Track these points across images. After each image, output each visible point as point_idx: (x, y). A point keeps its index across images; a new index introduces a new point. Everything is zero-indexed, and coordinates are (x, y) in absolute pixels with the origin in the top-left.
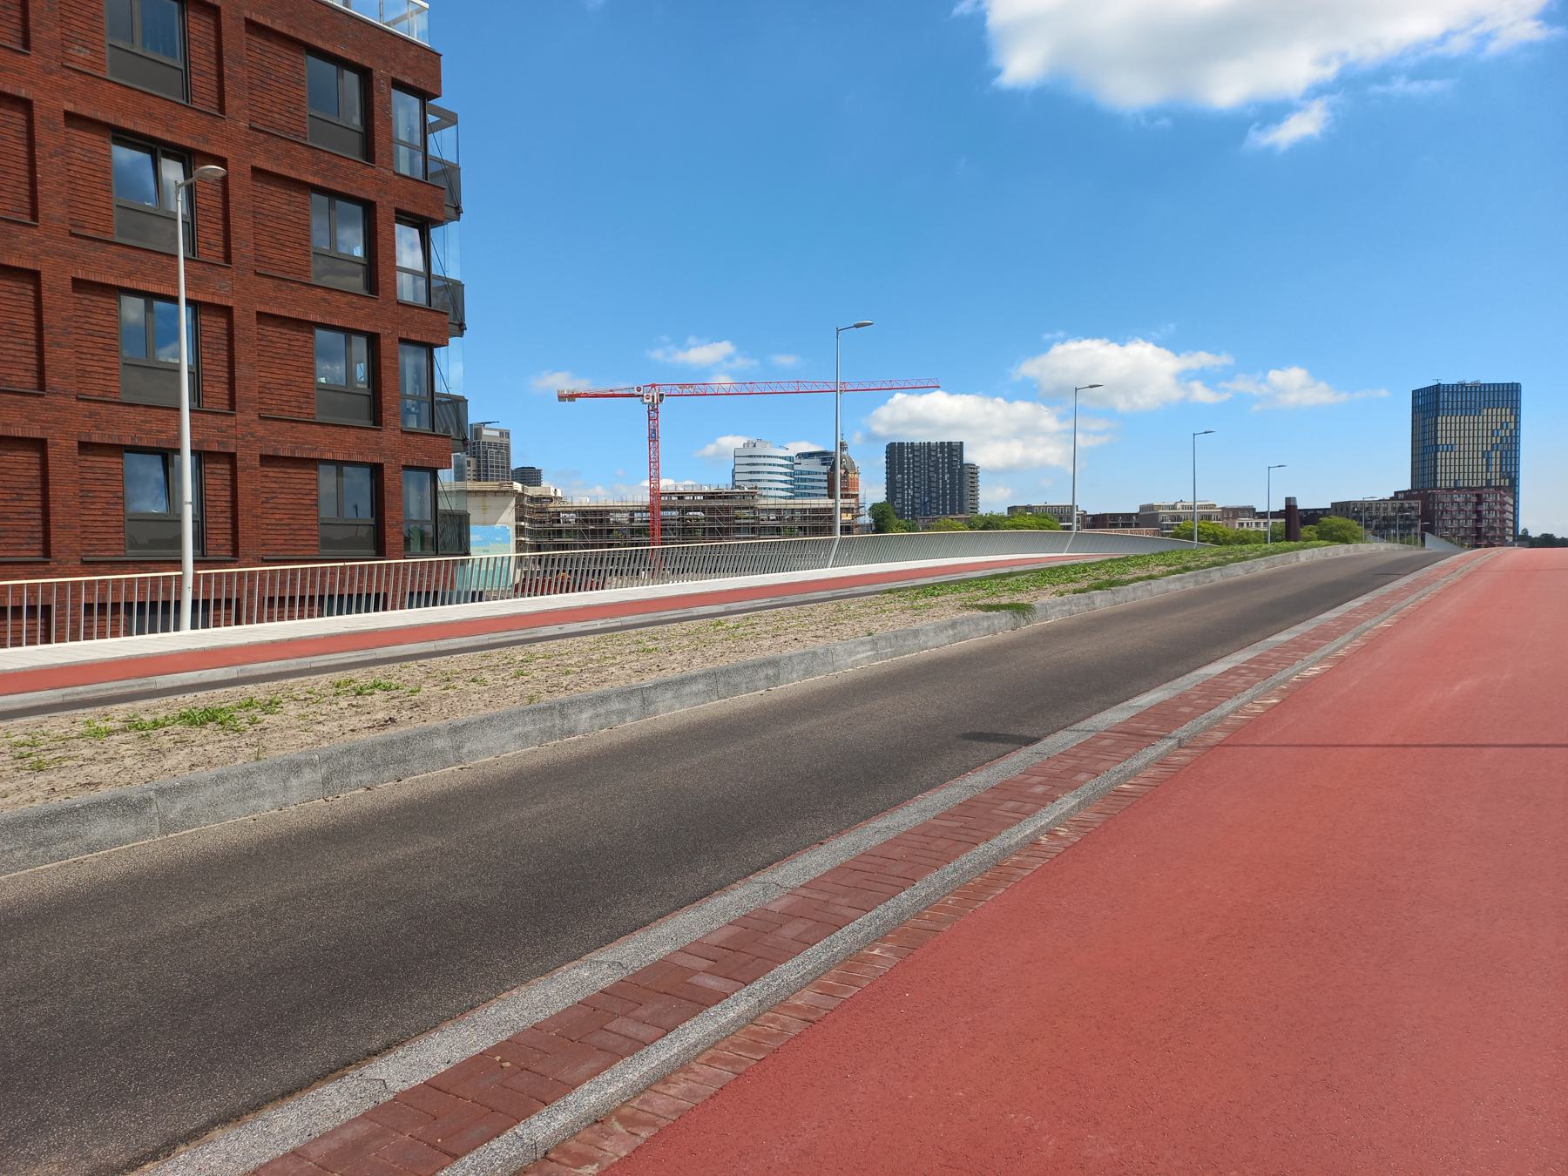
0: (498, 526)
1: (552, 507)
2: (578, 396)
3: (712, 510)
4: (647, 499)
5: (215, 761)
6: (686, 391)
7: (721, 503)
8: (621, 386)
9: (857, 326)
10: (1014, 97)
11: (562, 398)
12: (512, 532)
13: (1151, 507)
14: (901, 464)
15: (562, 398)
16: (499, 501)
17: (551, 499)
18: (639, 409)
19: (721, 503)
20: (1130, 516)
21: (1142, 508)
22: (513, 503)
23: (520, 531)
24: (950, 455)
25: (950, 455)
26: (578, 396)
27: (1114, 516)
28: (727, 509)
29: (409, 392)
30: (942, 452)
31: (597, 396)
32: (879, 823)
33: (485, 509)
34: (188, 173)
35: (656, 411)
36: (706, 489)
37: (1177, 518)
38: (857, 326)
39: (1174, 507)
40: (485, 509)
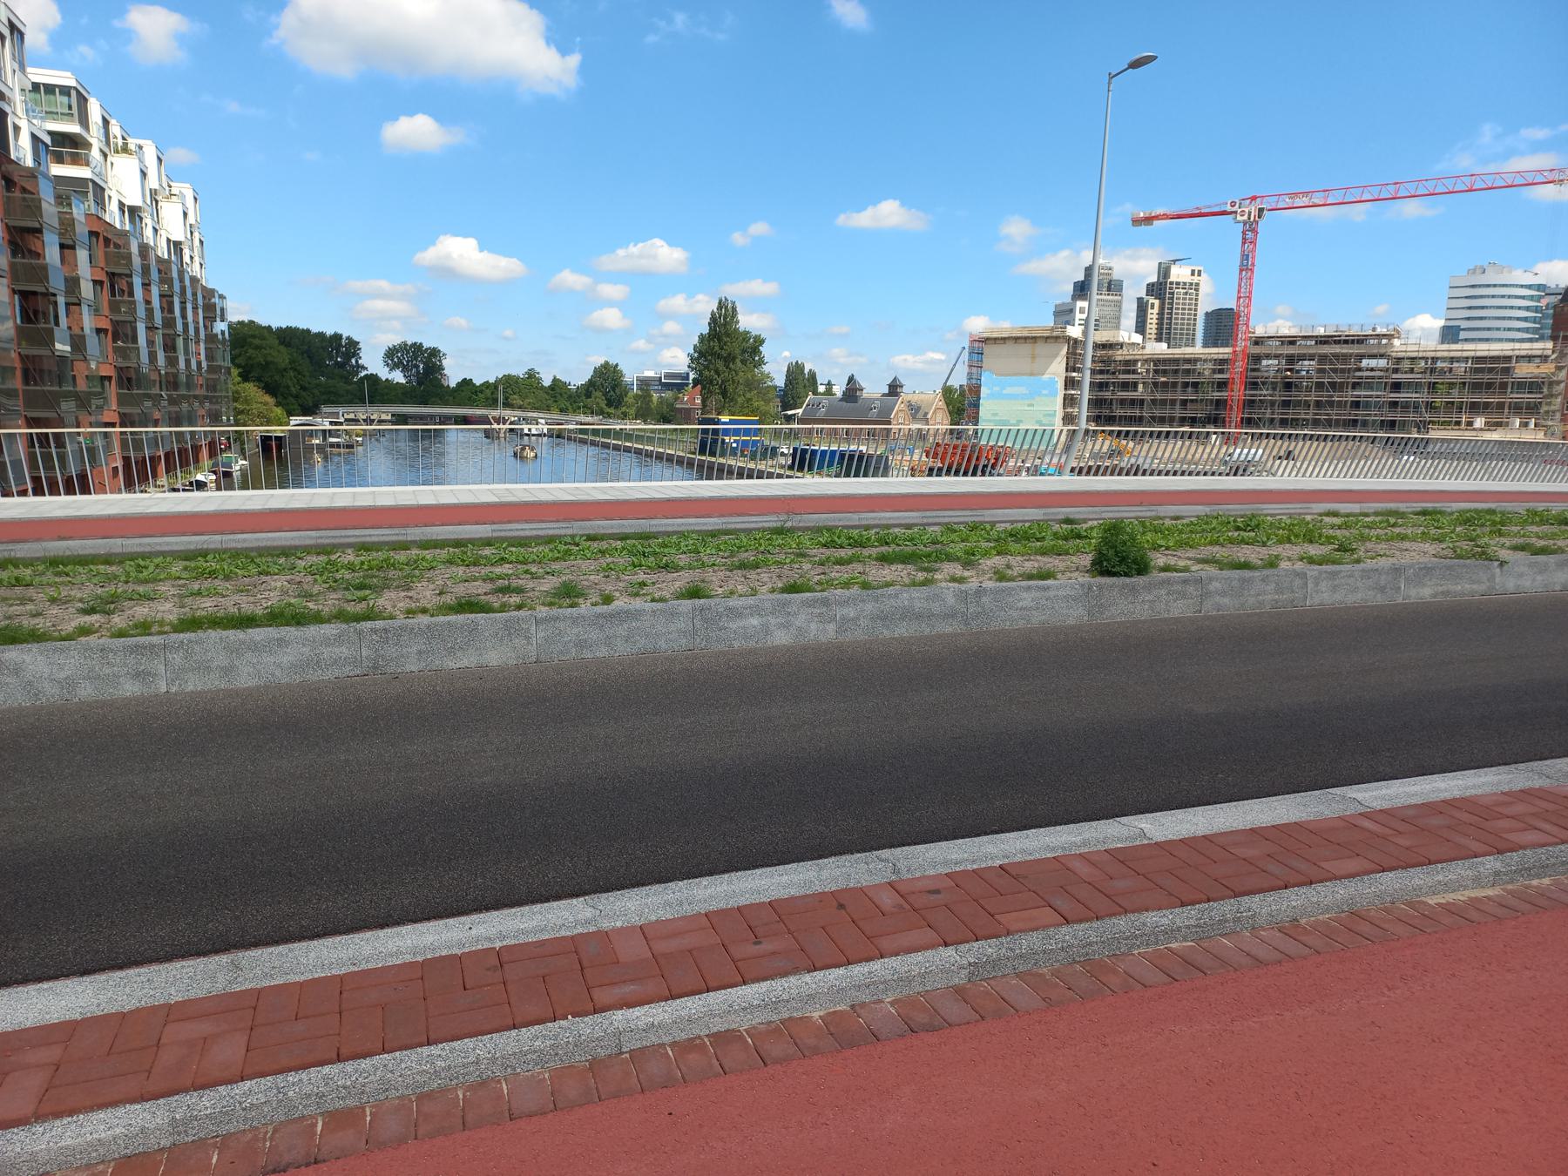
0: (1046, 377)
1: (1120, 355)
2: (1157, 217)
3: (1323, 358)
4: (677, 359)
5: (569, 622)
6: (1298, 202)
7: (1337, 349)
8: (1205, 204)
9: (1136, 64)
11: (1137, 222)
15: (1137, 222)
16: (1051, 347)
17: (1121, 345)
18: (1229, 231)
19: (1337, 349)
26: (1157, 217)
28: (1345, 358)
31: (1179, 217)
32: (437, 1051)
33: (1033, 357)
35: (1255, 231)
36: (1321, 331)
38: (1136, 64)
40: (1033, 357)
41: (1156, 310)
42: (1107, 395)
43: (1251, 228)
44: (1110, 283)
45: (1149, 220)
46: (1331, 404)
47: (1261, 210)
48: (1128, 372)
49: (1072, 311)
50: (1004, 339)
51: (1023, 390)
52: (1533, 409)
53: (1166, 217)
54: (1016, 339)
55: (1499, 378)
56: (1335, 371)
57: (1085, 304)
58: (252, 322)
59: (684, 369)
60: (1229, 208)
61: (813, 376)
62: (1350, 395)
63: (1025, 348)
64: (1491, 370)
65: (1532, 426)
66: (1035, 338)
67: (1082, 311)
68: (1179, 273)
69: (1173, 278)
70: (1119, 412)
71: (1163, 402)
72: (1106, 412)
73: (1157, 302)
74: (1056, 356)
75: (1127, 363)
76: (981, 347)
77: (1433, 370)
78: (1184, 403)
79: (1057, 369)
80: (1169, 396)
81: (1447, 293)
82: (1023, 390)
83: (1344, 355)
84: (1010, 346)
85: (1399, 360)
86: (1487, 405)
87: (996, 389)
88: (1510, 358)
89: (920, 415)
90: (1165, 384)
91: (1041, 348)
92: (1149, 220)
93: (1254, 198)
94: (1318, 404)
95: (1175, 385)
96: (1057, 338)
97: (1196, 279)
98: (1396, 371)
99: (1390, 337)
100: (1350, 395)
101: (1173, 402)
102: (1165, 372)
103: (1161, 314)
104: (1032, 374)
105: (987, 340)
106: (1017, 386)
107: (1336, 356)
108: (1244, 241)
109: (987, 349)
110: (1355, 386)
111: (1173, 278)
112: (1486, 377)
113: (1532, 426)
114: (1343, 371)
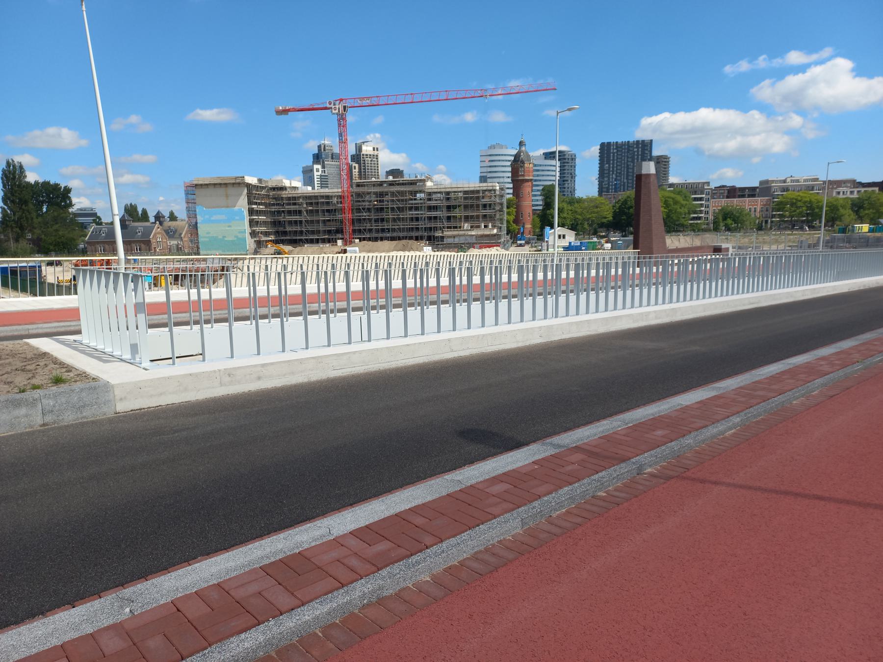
0: (236, 208)
2: (289, 110)
6: (365, 103)
10: (28, 183)
11: (279, 113)
12: (246, 213)
13: (767, 182)
14: (608, 157)
15: (279, 113)
20: (754, 189)
21: (761, 183)
22: (246, 191)
23: (251, 212)
24: (643, 150)
25: (643, 150)
27: (743, 189)
29: (340, 190)
30: (638, 147)
33: (227, 196)
34: (248, 186)
37: (785, 189)
39: (785, 181)
40: (227, 196)
41: (357, 170)
42: (281, 218)
43: (342, 118)
44: (332, 155)
45: (285, 112)
46: (399, 219)
47: (345, 107)
48: (295, 204)
49: (312, 170)
50: (207, 185)
51: (223, 217)
52: (491, 218)
53: (295, 110)
54: (215, 185)
55: (475, 202)
56: (398, 200)
57: (319, 167)
58: (46, 184)
59: (576, 196)
60: (328, 106)
61: (145, 212)
62: (409, 214)
63: (221, 191)
64: (471, 198)
65: (490, 227)
66: (226, 184)
67: (318, 170)
68: (367, 149)
69: (364, 152)
70: (288, 229)
71: (312, 222)
72: (281, 229)
73: (357, 166)
74: (241, 195)
75: (289, 199)
76: (194, 190)
77: (448, 199)
78: (324, 221)
79: (242, 203)
80: (315, 218)
81: (479, 159)
82: (223, 217)
83: (402, 192)
84: (211, 190)
85: (430, 194)
86: (472, 217)
87: (207, 217)
88: (478, 192)
89: (177, 235)
90: (311, 211)
91: (231, 190)
92: (285, 112)
93: (341, 100)
94: (394, 220)
95: (317, 211)
96: (239, 184)
97: (376, 153)
98: (430, 200)
99: (424, 181)
100: (409, 214)
101: (318, 222)
102: (311, 204)
103: (360, 172)
104: (228, 207)
105: (196, 185)
106: (219, 215)
107: (398, 192)
108: (339, 125)
109: (197, 191)
110: (411, 209)
111: (364, 152)
112: (469, 202)
113: (490, 227)
114: (402, 200)
